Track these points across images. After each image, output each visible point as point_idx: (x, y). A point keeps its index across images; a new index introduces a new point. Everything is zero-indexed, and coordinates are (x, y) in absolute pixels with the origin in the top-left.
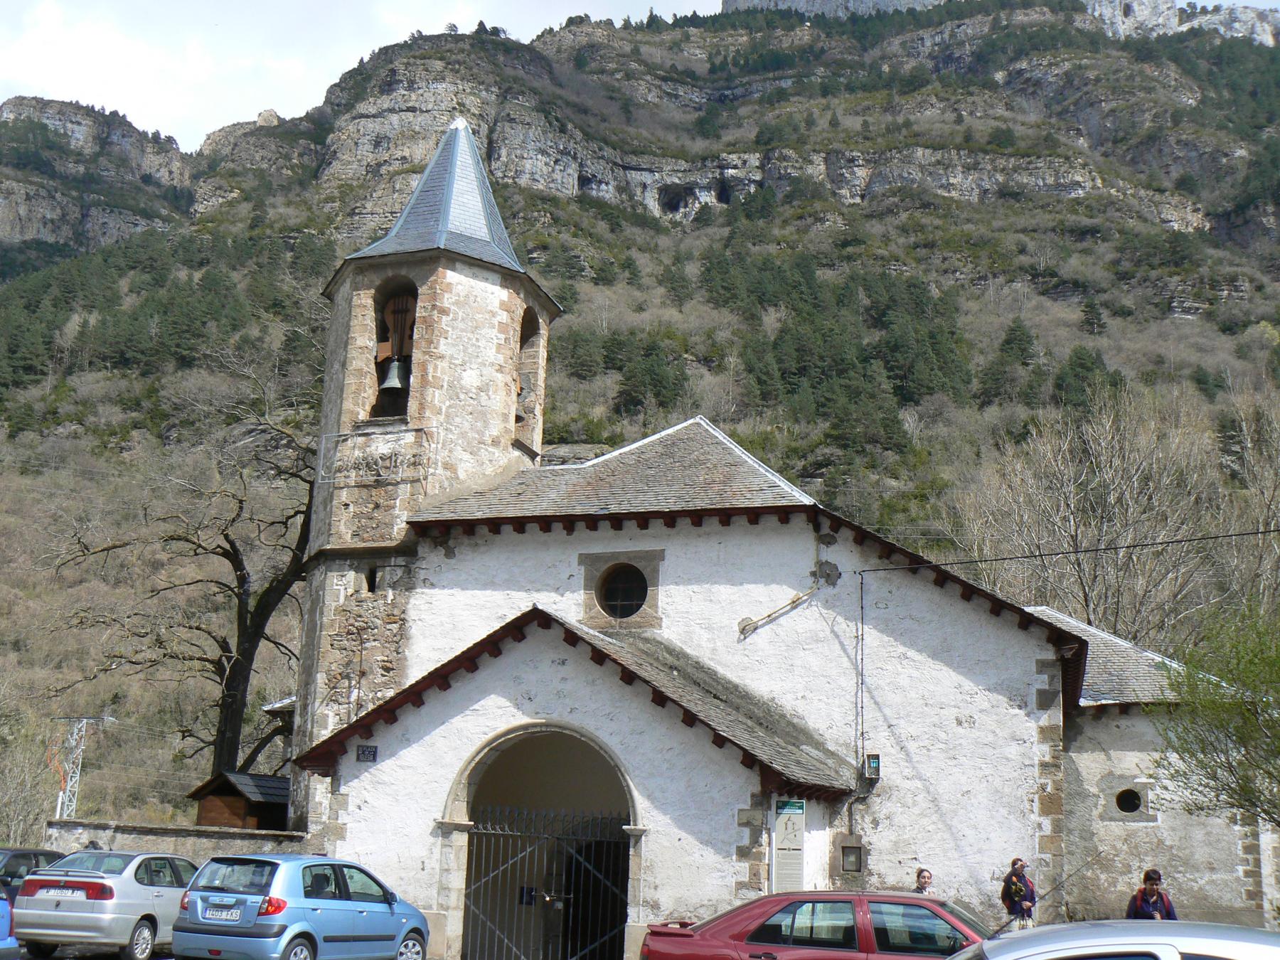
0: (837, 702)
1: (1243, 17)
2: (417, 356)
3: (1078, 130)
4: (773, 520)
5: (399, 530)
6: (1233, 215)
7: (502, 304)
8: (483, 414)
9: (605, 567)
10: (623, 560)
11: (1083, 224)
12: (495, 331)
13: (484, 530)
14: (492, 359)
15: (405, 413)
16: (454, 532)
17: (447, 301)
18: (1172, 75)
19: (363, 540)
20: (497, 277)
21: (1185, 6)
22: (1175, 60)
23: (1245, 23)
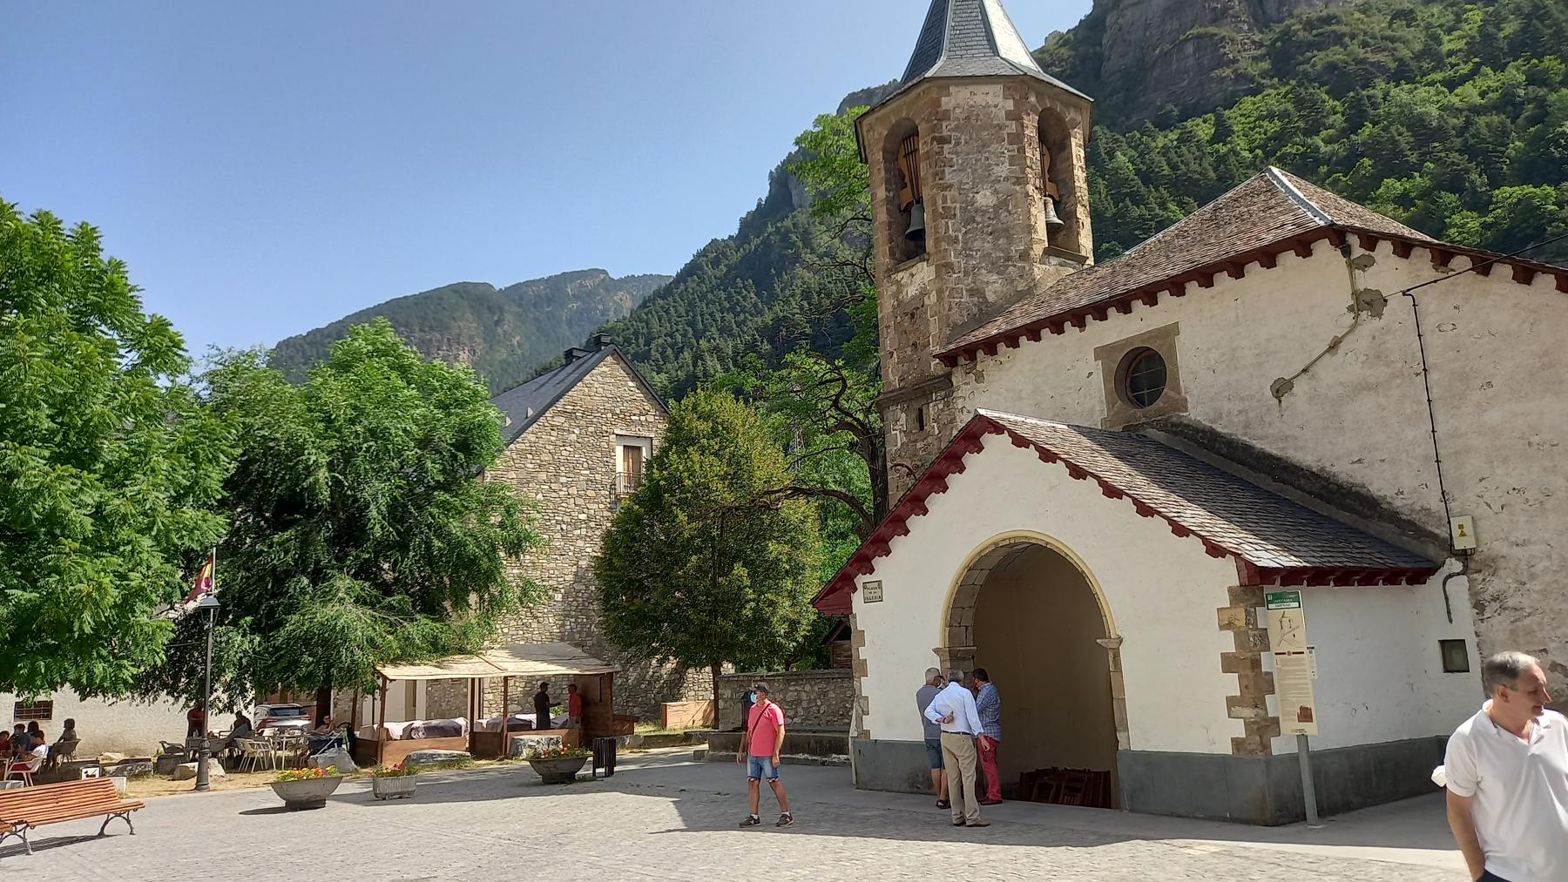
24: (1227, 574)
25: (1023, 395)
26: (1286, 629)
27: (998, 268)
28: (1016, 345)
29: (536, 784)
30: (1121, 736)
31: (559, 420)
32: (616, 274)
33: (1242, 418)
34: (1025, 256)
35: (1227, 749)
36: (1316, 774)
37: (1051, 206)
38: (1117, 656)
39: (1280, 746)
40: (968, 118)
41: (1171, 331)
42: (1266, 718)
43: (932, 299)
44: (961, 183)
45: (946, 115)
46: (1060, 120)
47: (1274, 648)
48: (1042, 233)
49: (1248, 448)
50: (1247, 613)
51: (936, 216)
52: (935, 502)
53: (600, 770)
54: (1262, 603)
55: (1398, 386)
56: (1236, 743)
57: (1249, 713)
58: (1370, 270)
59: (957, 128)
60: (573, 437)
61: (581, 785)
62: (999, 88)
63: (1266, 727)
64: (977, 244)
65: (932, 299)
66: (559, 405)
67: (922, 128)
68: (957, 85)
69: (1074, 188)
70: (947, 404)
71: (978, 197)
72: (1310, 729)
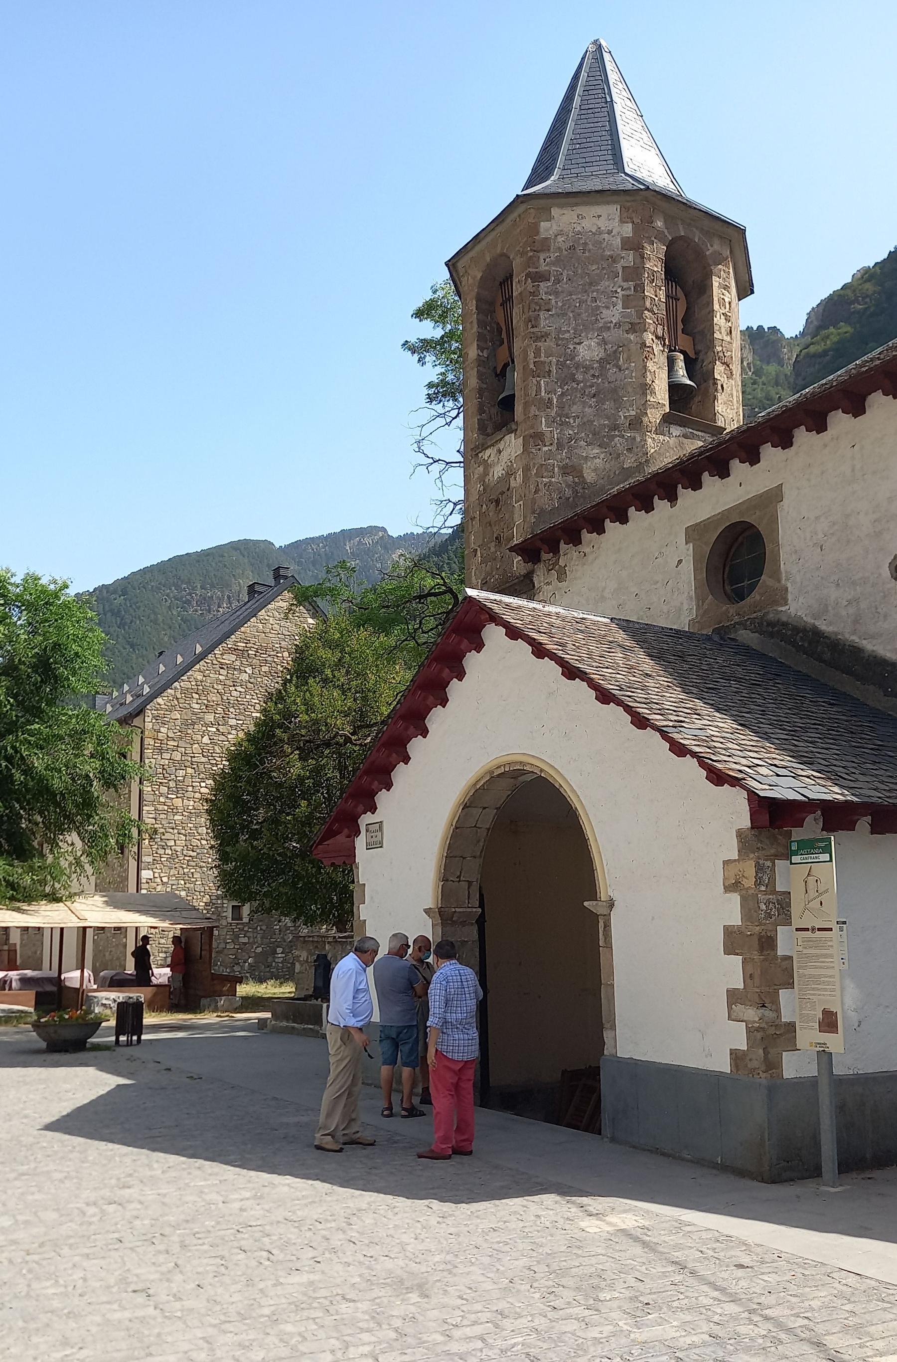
24: (735, 811)
26: (812, 893)
27: (600, 439)
28: (601, 530)
29: (39, 1052)
30: (607, 1035)
31: (229, 658)
32: (394, 532)
33: (851, 610)
34: (636, 423)
35: (725, 1066)
36: (841, 1109)
37: (680, 364)
38: (607, 926)
39: (795, 1066)
40: (572, 248)
41: (775, 496)
42: (776, 1023)
43: (517, 481)
44: (559, 331)
45: (545, 245)
46: (699, 254)
47: (796, 922)
48: (661, 394)
49: (856, 651)
50: (759, 868)
51: (529, 374)
52: (437, 719)
53: (123, 1038)
54: (787, 855)
56: (736, 1056)
57: (752, 1014)
59: (558, 261)
60: (245, 677)
61: (92, 1054)
62: (613, 210)
63: (774, 1037)
64: (576, 409)
65: (517, 481)
66: (230, 643)
67: (517, 263)
68: (561, 206)
69: (713, 340)
71: (580, 348)
72: (835, 1043)
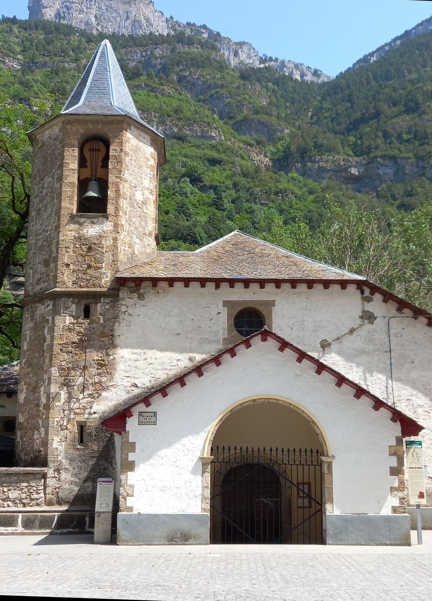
0: (378, 386)
1: (288, 65)
2: (112, 178)
3: (214, 110)
4: (337, 287)
5: (106, 280)
6: (282, 161)
7: (151, 154)
8: (145, 217)
9: (239, 309)
10: (251, 305)
11: (215, 157)
12: (149, 169)
13: (165, 284)
14: (147, 186)
15: (106, 212)
16: (143, 284)
17: (127, 147)
18: (257, 89)
19: (81, 286)
20: (148, 138)
21: (262, 56)
22: (258, 80)
23: (289, 68)
25: (172, 314)
55: (377, 355)
58: (371, 303)
68: (135, 126)
70: (113, 307)
